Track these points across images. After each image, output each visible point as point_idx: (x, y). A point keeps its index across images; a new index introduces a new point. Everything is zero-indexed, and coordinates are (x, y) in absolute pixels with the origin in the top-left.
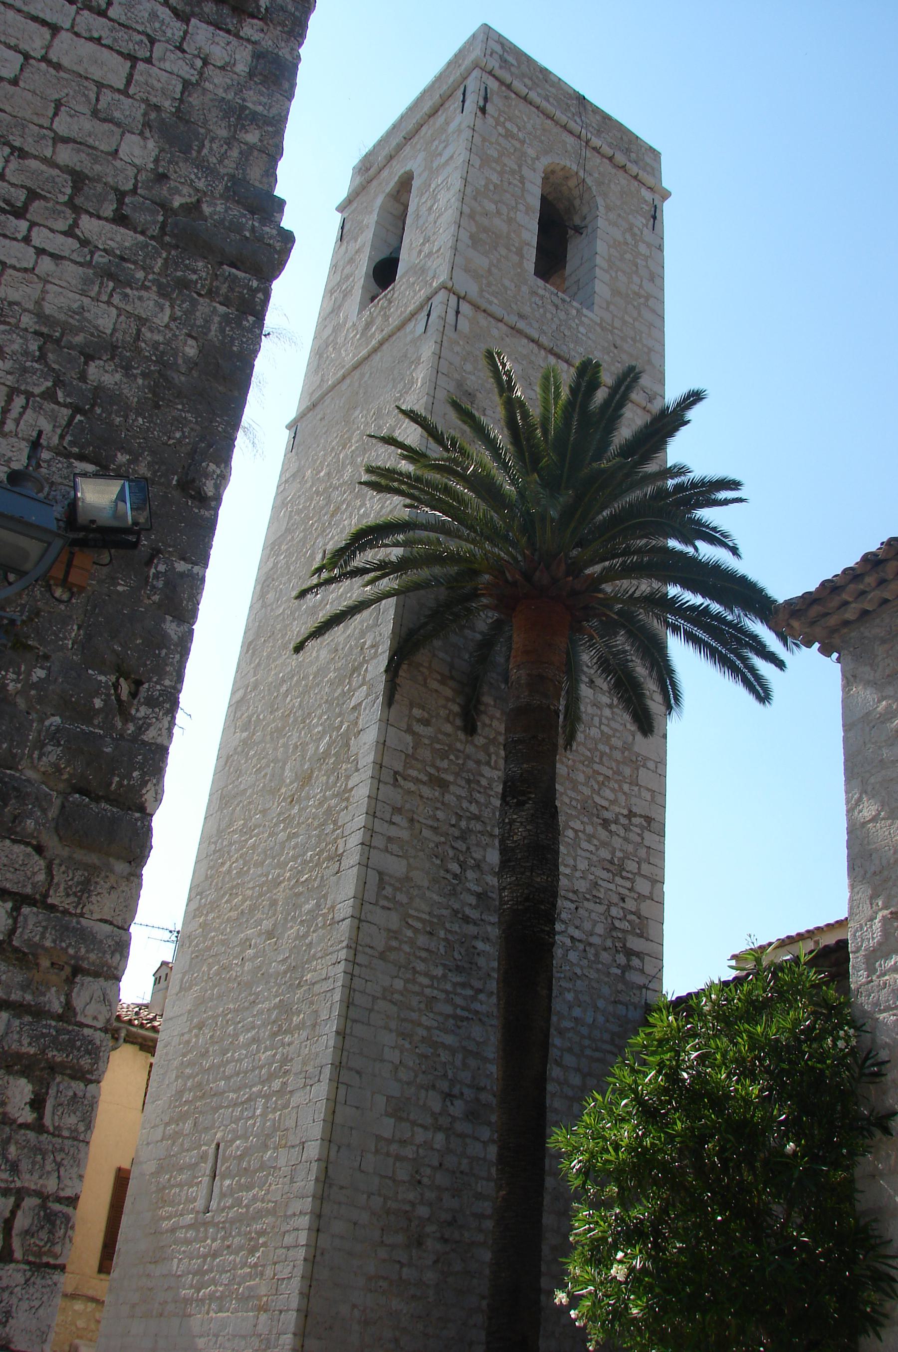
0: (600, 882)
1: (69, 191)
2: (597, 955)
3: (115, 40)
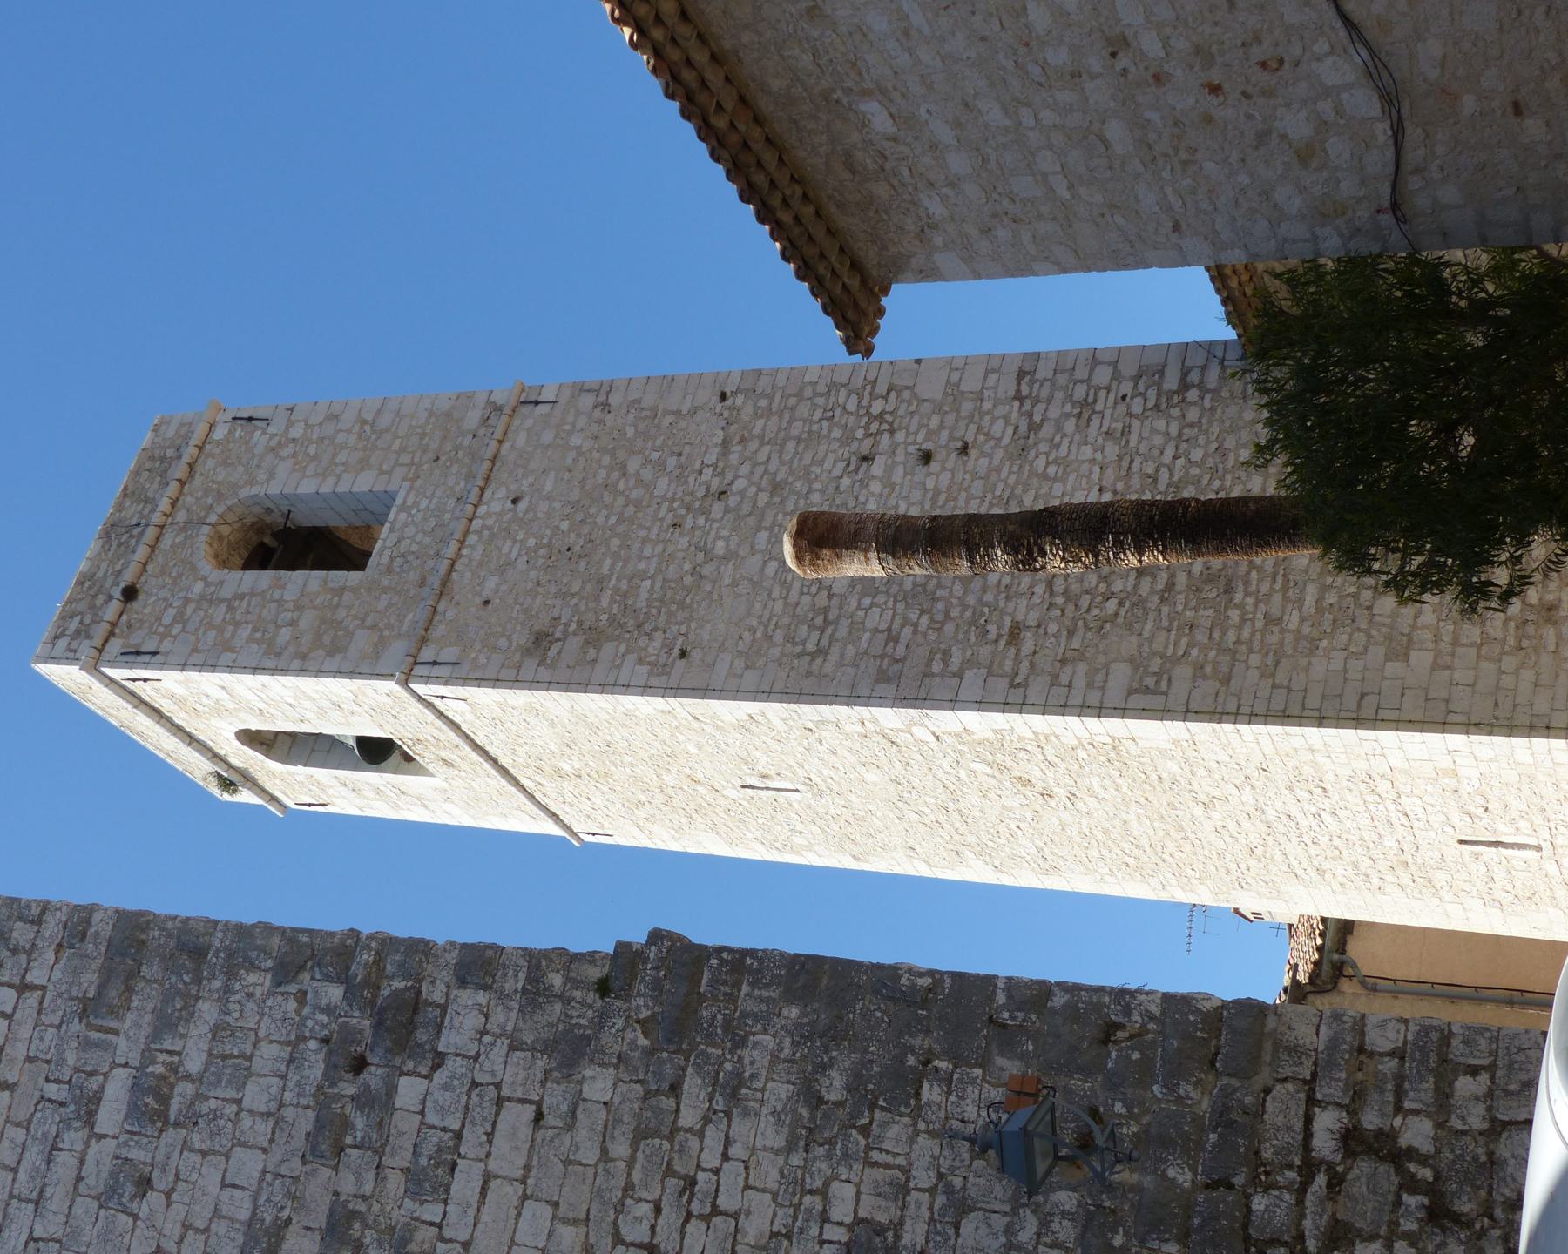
0: (1104, 429)
1: (657, 1141)
2: (1192, 425)
3: (485, 1119)
